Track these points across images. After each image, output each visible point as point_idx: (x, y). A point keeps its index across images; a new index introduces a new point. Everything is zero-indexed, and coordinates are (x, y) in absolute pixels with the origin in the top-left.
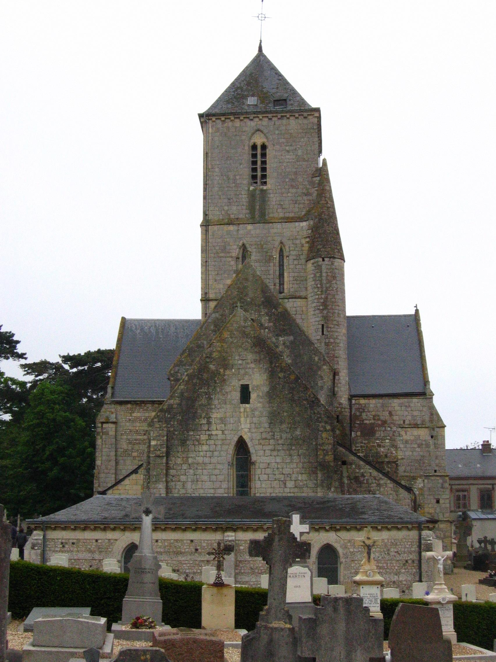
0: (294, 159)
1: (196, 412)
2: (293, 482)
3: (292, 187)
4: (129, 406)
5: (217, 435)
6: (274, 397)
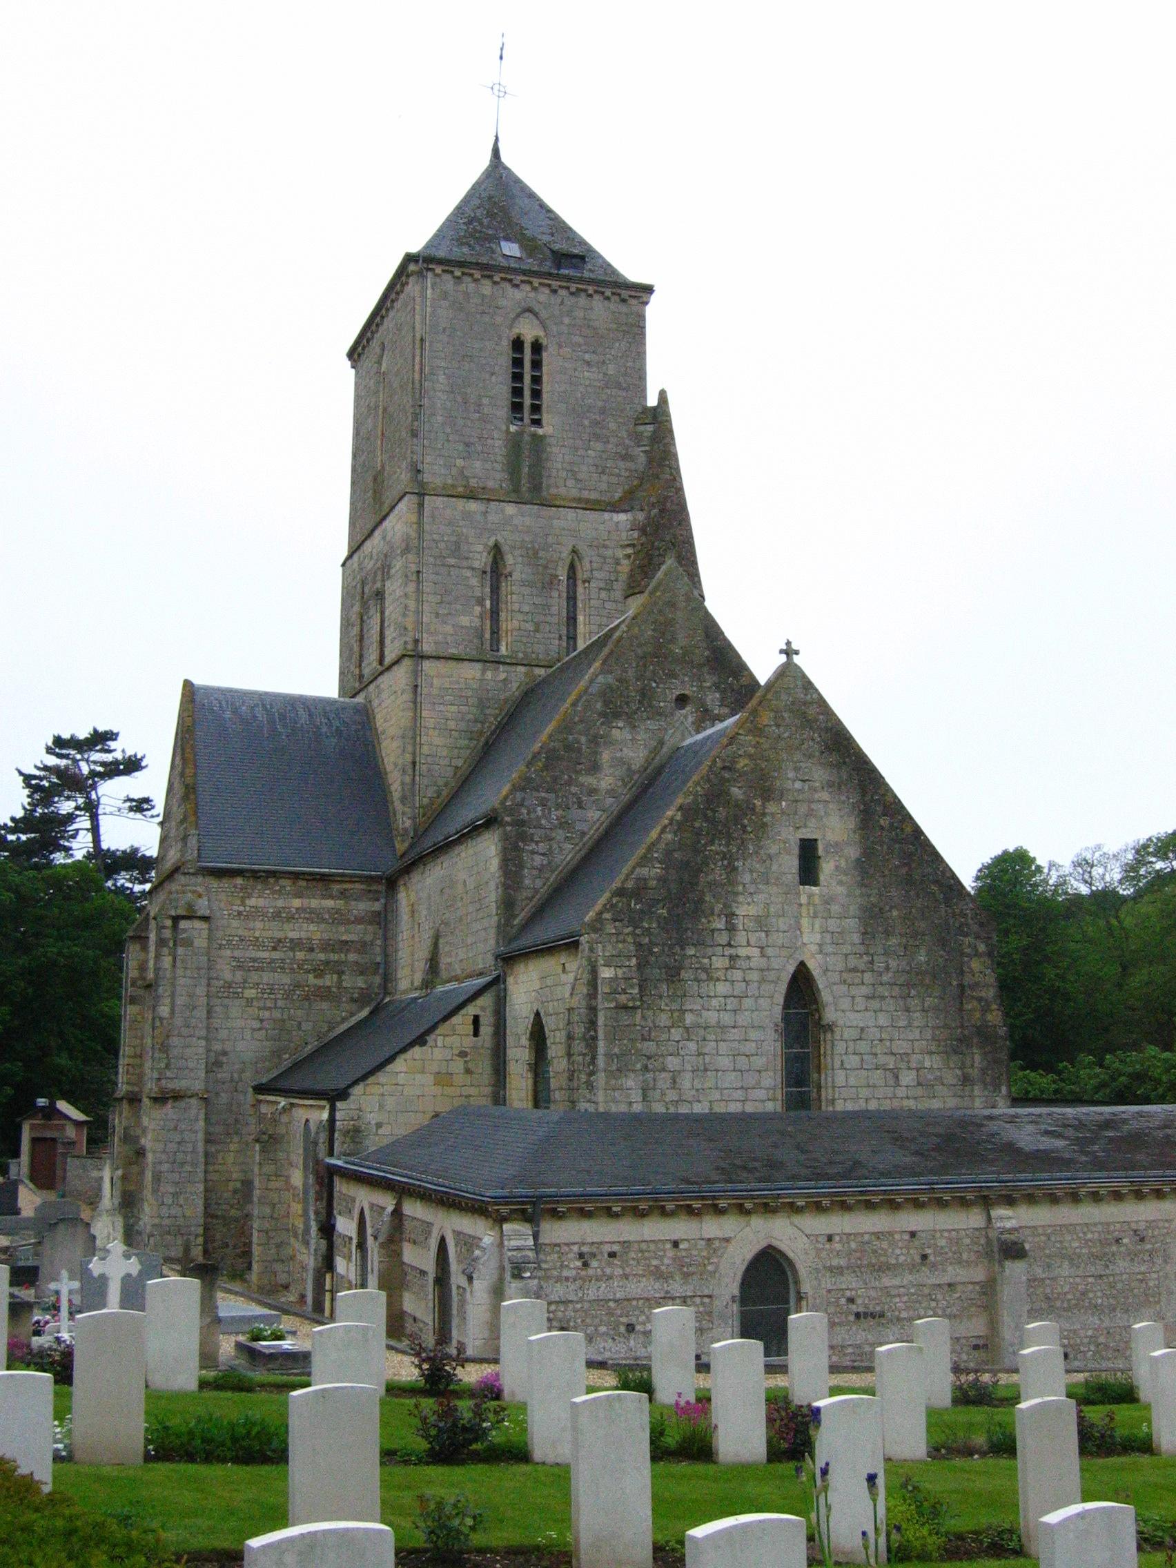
0: (599, 381)
1: (701, 900)
2: (914, 1073)
3: (597, 437)
4: (239, 881)
5: (748, 958)
6: (872, 871)
